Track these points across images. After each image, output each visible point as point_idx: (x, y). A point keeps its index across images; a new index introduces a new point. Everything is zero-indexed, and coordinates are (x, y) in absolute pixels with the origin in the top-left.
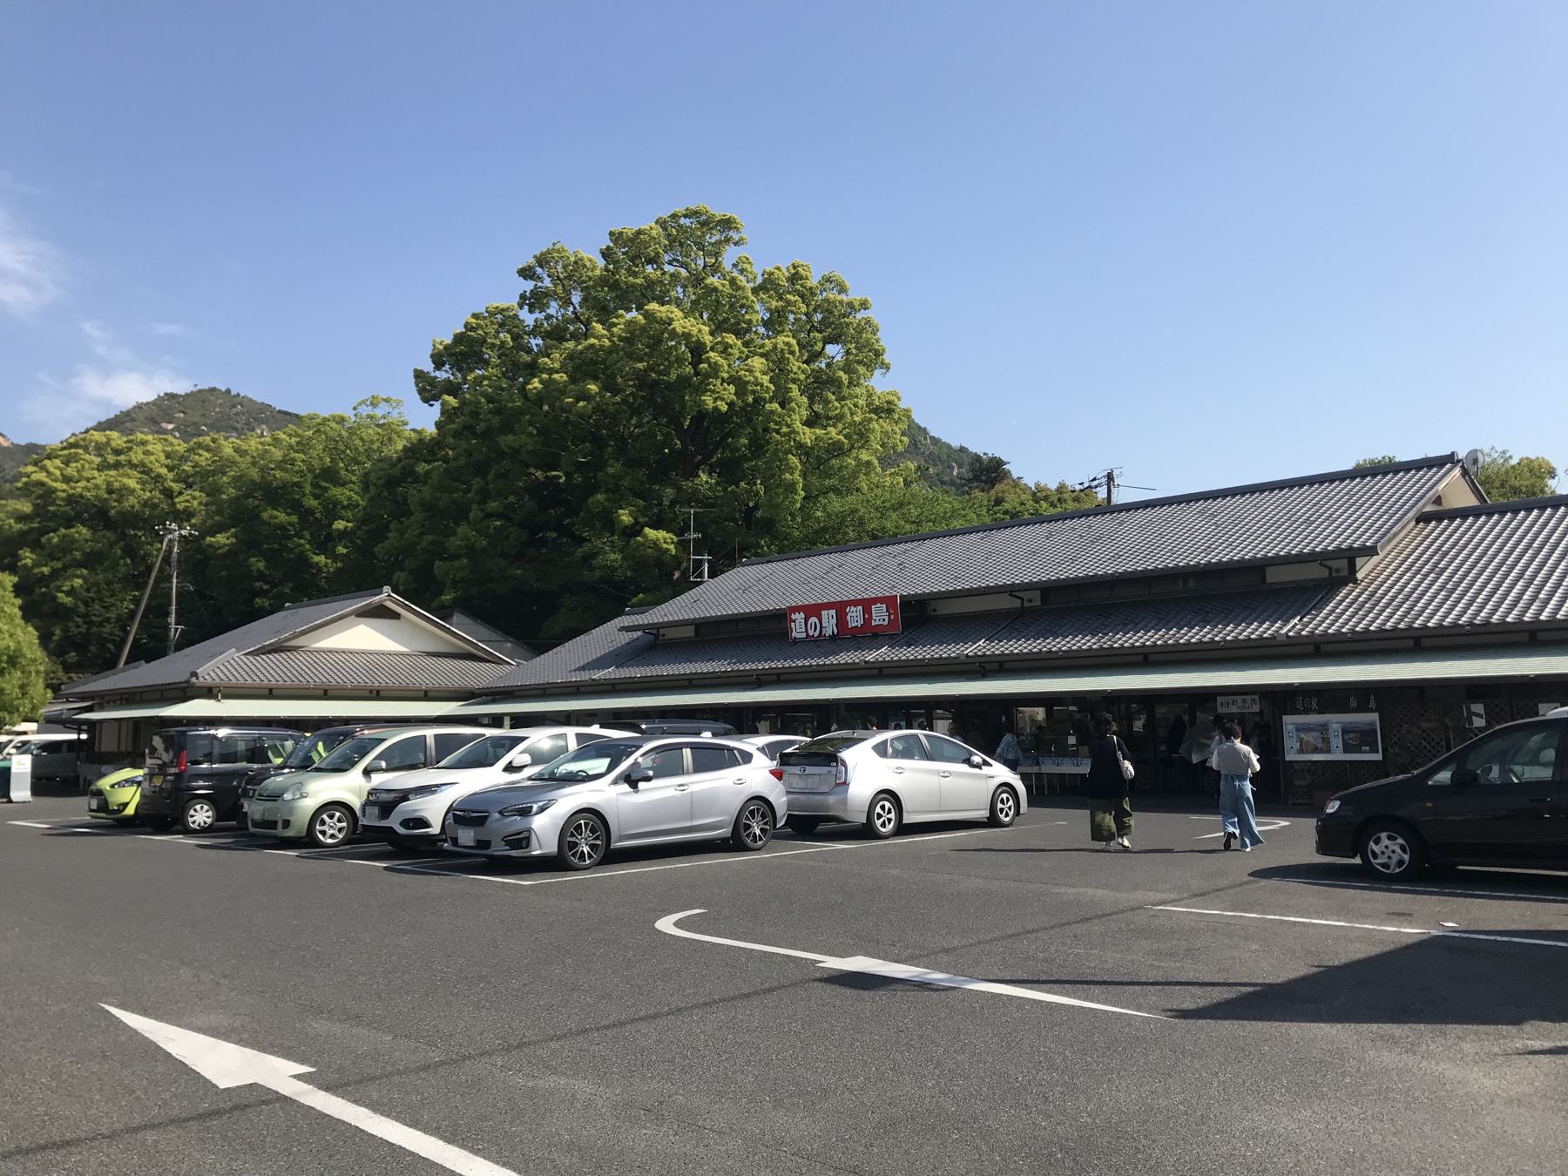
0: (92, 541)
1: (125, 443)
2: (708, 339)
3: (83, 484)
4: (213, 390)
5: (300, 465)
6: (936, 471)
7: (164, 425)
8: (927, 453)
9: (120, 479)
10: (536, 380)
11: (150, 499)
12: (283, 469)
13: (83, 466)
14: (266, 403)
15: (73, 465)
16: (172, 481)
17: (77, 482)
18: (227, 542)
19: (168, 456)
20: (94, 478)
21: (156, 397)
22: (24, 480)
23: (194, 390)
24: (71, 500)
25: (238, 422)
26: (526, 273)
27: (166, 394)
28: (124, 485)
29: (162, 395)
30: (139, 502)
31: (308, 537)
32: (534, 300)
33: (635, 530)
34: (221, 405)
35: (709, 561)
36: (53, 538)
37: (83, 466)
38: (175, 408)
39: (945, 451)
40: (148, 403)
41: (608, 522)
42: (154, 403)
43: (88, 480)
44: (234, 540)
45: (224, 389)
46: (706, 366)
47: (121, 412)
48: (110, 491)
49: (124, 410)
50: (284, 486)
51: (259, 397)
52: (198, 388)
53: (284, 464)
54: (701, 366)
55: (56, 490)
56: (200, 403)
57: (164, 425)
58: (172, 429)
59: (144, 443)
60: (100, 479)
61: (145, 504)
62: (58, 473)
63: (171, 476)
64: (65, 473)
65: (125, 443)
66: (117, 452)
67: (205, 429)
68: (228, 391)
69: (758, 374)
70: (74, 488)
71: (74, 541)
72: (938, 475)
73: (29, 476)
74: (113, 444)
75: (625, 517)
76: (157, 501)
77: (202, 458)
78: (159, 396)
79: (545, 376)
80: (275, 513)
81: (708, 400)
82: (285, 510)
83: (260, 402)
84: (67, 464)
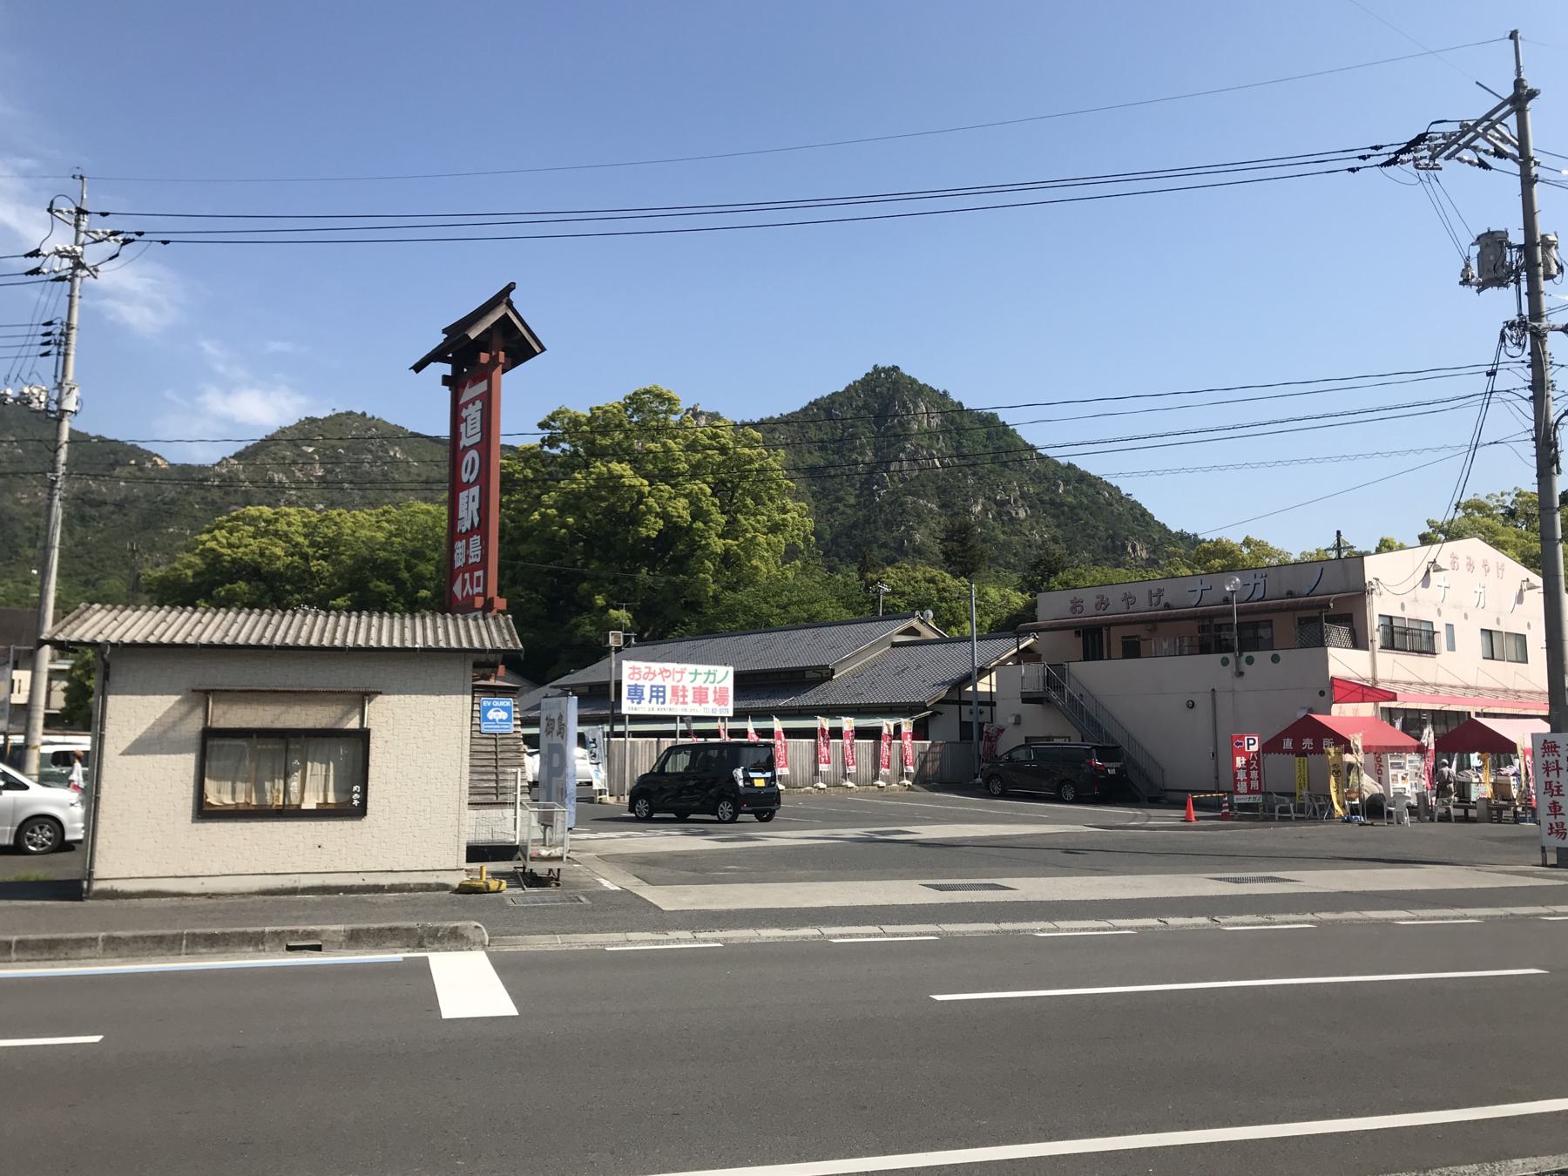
0: (249, 594)
1: (273, 514)
2: (647, 489)
3: (242, 550)
4: (350, 413)
5: (397, 547)
6: (1036, 491)
7: (304, 448)
8: (1033, 470)
9: (270, 547)
10: (536, 513)
11: (292, 562)
12: (384, 550)
13: (242, 535)
14: (399, 425)
15: (235, 534)
16: (308, 547)
17: (238, 548)
18: (345, 604)
19: (305, 525)
20: (250, 545)
21: (298, 421)
22: (201, 547)
23: (332, 414)
24: (234, 561)
25: (373, 445)
26: (542, 426)
27: (307, 418)
28: (273, 553)
29: (303, 419)
30: (283, 565)
31: (402, 601)
32: (552, 441)
33: (604, 610)
34: (356, 428)
35: (635, 637)
36: (220, 592)
37: (242, 535)
38: (314, 431)
39: (1052, 467)
40: (290, 427)
41: (588, 607)
42: (295, 427)
43: (246, 546)
44: (349, 603)
45: (359, 412)
46: (643, 507)
47: (266, 436)
48: (262, 554)
49: (269, 434)
50: (387, 562)
51: (393, 420)
52: (336, 412)
53: (383, 547)
54: (641, 507)
55: (223, 555)
56: (338, 427)
57: (304, 448)
58: (312, 452)
59: (288, 515)
60: (255, 545)
61: (288, 567)
62: (224, 541)
63: (307, 542)
64: (230, 541)
65: (273, 514)
66: (268, 522)
67: (342, 451)
68: (364, 414)
69: (681, 511)
70: (236, 553)
71: (235, 594)
72: (1038, 494)
73: (204, 544)
74: (264, 516)
75: (600, 600)
76: (296, 564)
77: (330, 531)
78: (300, 420)
79: (543, 510)
80: (379, 583)
81: (643, 531)
82: (386, 580)
83: (393, 424)
84: (231, 532)
